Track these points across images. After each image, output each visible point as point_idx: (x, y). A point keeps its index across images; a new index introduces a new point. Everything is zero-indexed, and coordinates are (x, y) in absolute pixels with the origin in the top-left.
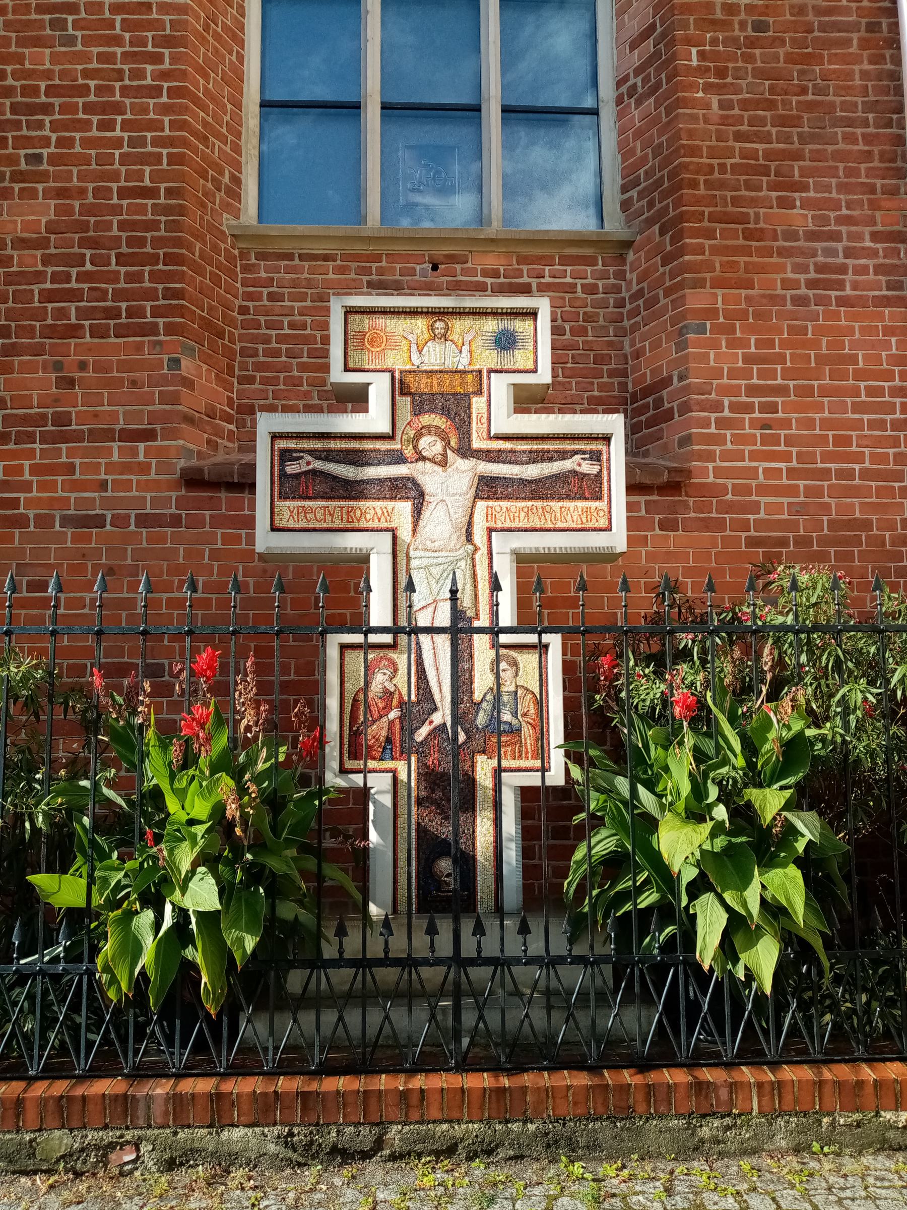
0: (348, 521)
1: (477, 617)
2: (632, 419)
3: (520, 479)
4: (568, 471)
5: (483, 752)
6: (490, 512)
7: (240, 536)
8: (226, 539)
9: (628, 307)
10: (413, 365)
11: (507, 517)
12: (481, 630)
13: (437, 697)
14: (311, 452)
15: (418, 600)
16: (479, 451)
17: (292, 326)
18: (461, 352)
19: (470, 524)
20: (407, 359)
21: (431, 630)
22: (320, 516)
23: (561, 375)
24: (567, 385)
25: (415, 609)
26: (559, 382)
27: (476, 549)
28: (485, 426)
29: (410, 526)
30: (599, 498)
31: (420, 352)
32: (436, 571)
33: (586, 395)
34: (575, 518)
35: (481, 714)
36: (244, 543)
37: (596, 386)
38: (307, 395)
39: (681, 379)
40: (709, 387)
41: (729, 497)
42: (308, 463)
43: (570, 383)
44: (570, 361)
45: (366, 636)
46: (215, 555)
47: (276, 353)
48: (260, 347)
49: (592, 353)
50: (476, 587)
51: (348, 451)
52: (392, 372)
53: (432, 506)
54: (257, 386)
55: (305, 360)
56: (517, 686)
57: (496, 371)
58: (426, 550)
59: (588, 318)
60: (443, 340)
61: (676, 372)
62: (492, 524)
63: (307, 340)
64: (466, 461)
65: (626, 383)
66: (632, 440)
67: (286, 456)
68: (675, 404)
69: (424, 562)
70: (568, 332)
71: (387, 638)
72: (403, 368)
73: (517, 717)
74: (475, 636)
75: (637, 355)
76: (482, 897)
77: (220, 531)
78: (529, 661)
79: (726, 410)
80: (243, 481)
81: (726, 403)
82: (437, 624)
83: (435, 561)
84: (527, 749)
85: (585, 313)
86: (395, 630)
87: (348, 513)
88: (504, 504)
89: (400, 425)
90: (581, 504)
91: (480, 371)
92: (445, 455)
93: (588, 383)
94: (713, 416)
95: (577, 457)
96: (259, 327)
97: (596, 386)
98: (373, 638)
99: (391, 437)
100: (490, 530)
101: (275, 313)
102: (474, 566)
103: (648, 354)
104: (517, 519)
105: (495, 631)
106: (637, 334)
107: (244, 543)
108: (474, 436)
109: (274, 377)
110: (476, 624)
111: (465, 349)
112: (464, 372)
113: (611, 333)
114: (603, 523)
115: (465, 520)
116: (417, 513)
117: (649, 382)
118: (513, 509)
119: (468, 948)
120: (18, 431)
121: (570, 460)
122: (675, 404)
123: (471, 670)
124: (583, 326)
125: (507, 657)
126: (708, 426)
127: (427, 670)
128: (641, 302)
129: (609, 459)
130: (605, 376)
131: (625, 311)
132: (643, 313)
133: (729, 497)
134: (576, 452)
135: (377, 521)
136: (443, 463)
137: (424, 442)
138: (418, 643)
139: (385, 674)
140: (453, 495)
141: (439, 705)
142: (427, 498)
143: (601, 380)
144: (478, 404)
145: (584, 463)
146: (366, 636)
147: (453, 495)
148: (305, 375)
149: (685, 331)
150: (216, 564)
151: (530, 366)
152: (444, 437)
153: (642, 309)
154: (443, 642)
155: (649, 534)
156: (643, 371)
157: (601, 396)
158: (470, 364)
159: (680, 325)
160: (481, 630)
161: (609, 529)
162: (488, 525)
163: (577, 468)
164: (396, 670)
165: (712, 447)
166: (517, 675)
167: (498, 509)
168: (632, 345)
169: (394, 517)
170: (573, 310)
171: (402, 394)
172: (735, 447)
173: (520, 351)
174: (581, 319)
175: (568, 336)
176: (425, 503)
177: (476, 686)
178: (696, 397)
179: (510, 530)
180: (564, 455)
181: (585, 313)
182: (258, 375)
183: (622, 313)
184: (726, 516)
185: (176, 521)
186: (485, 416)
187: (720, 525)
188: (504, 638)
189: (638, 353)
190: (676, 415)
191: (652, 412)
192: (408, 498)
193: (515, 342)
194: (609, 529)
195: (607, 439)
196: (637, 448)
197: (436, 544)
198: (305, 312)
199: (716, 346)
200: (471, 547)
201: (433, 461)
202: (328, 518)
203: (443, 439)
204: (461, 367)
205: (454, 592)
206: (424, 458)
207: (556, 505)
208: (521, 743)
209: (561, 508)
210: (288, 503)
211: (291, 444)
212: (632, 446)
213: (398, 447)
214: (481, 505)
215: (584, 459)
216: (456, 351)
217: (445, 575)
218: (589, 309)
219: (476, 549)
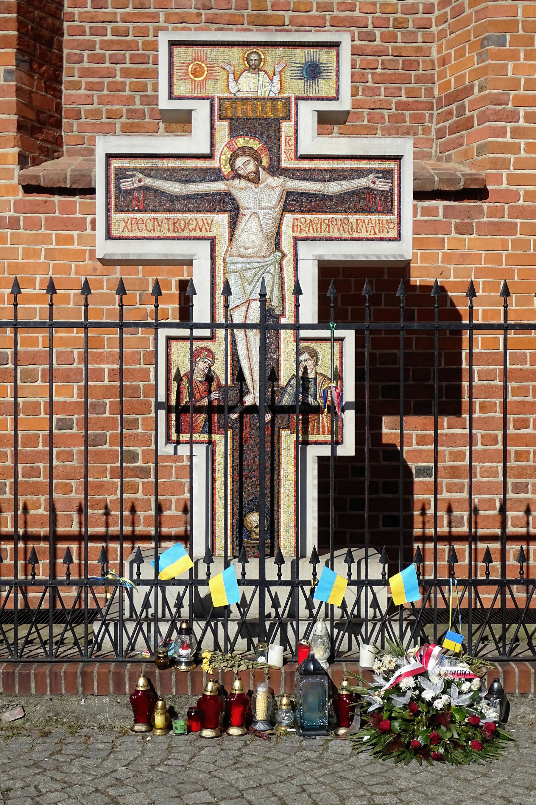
0: (174, 231)
1: (284, 315)
2: (438, 123)
3: (322, 194)
4: (364, 188)
5: (288, 428)
6: (296, 224)
7: (72, 237)
8: (60, 240)
9: (437, 13)
10: (231, 93)
11: (311, 228)
12: (286, 327)
13: (249, 382)
14: (142, 171)
15: (233, 301)
16: (287, 170)
17: (115, 33)
18: (272, 80)
19: (278, 234)
20: (225, 88)
21: (244, 326)
22: (150, 227)
23: (370, 80)
24: (376, 91)
25: (231, 307)
26: (369, 88)
27: (284, 256)
28: (293, 147)
29: (226, 236)
30: (390, 211)
31: (236, 81)
32: (249, 274)
33: (394, 100)
34: (369, 229)
35: (286, 397)
36: (76, 243)
37: (403, 91)
38: (130, 100)
39: (481, 89)
40: (506, 98)
41: (521, 202)
42: (140, 181)
43: (379, 88)
44: (380, 66)
45: (191, 330)
46: (50, 254)
47: (101, 60)
48: (86, 53)
49: (401, 59)
50: (283, 288)
51: (174, 170)
52: (212, 100)
53: (245, 218)
54: (82, 91)
55: (128, 65)
56: (316, 373)
57: (304, 99)
58: (240, 256)
59: (399, 24)
60: (257, 70)
61: (477, 82)
62: (297, 234)
63: (130, 46)
64: (276, 178)
65: (432, 89)
66: (437, 145)
67: (121, 174)
68: (475, 113)
69: (238, 267)
70: (378, 38)
71: (207, 332)
72: (222, 95)
73: (316, 400)
74: (282, 331)
75: (444, 61)
76: (284, 544)
77: (54, 233)
78: (323, 349)
79: (522, 120)
80: (75, 186)
81: (522, 113)
82: (249, 321)
83: (248, 266)
84: (323, 426)
85: (395, 19)
86: (213, 325)
87: (174, 224)
88: (308, 216)
89: (220, 146)
90: (375, 217)
91: (288, 99)
92: (257, 173)
93: (397, 88)
94: (509, 126)
95: (372, 176)
96: (83, 34)
97: (403, 91)
98: (197, 332)
99: (210, 157)
100: (296, 239)
101: (98, 19)
102: (281, 270)
103: (453, 62)
104: (319, 230)
105: (297, 327)
106: (444, 41)
107: (76, 243)
108: (283, 157)
109: (98, 83)
110: (283, 321)
111: (276, 78)
112: (274, 99)
113: (420, 39)
114: (393, 234)
115: (274, 230)
116: (233, 224)
117: (453, 89)
118: (316, 221)
119: (271, 574)
120: (465, 454)
121: (366, 179)
122: (475, 113)
123: (278, 360)
124: (393, 32)
125: (307, 350)
126: (504, 135)
127: (240, 359)
128: (448, 9)
129: (399, 178)
130: (413, 81)
131: (433, 17)
132: (450, 21)
133: (521, 202)
134: (371, 171)
135: (198, 230)
136: (255, 180)
137: (240, 161)
138: (233, 336)
139: (205, 362)
140: (264, 208)
141: (251, 388)
142: (242, 211)
143: (409, 85)
144: (286, 127)
145: (377, 181)
146: (191, 330)
147: (264, 208)
148: (128, 81)
149: (486, 42)
150: (51, 263)
151: (333, 94)
152: (255, 156)
153: (449, 17)
154: (254, 336)
155: (446, 237)
156: (448, 78)
157: (408, 102)
158: (279, 93)
159: (482, 37)
160: (286, 327)
161: (398, 239)
162: (294, 235)
163: (371, 185)
164: (214, 359)
165: (507, 156)
166: (316, 364)
167: (303, 221)
168: (439, 51)
169: (214, 229)
170: (384, 16)
171: (220, 119)
172: (528, 156)
173: (324, 81)
174: (391, 25)
175: (378, 42)
176: (240, 216)
177: (282, 373)
178: (494, 107)
179: (314, 239)
180: (361, 173)
181: (395, 19)
182: (84, 80)
183: (431, 19)
184: (517, 220)
185: (14, 223)
186: (293, 138)
187: (511, 229)
188: (303, 333)
189: (444, 60)
190: (476, 123)
191: (455, 119)
192: (225, 211)
193: (319, 72)
194: (398, 239)
195: (398, 158)
196: (441, 153)
197: (249, 251)
198: (127, 19)
199: (514, 57)
200: (279, 254)
201: (246, 178)
202: (157, 228)
203: (256, 159)
204: (272, 95)
205: (263, 295)
206: (240, 176)
207: (353, 218)
208: (319, 421)
209: (357, 220)
210: (123, 215)
211: (125, 163)
212: (436, 150)
213: (217, 165)
214: (288, 218)
215: (378, 178)
216: (268, 80)
217: (257, 278)
218: (399, 15)
219: (284, 256)
